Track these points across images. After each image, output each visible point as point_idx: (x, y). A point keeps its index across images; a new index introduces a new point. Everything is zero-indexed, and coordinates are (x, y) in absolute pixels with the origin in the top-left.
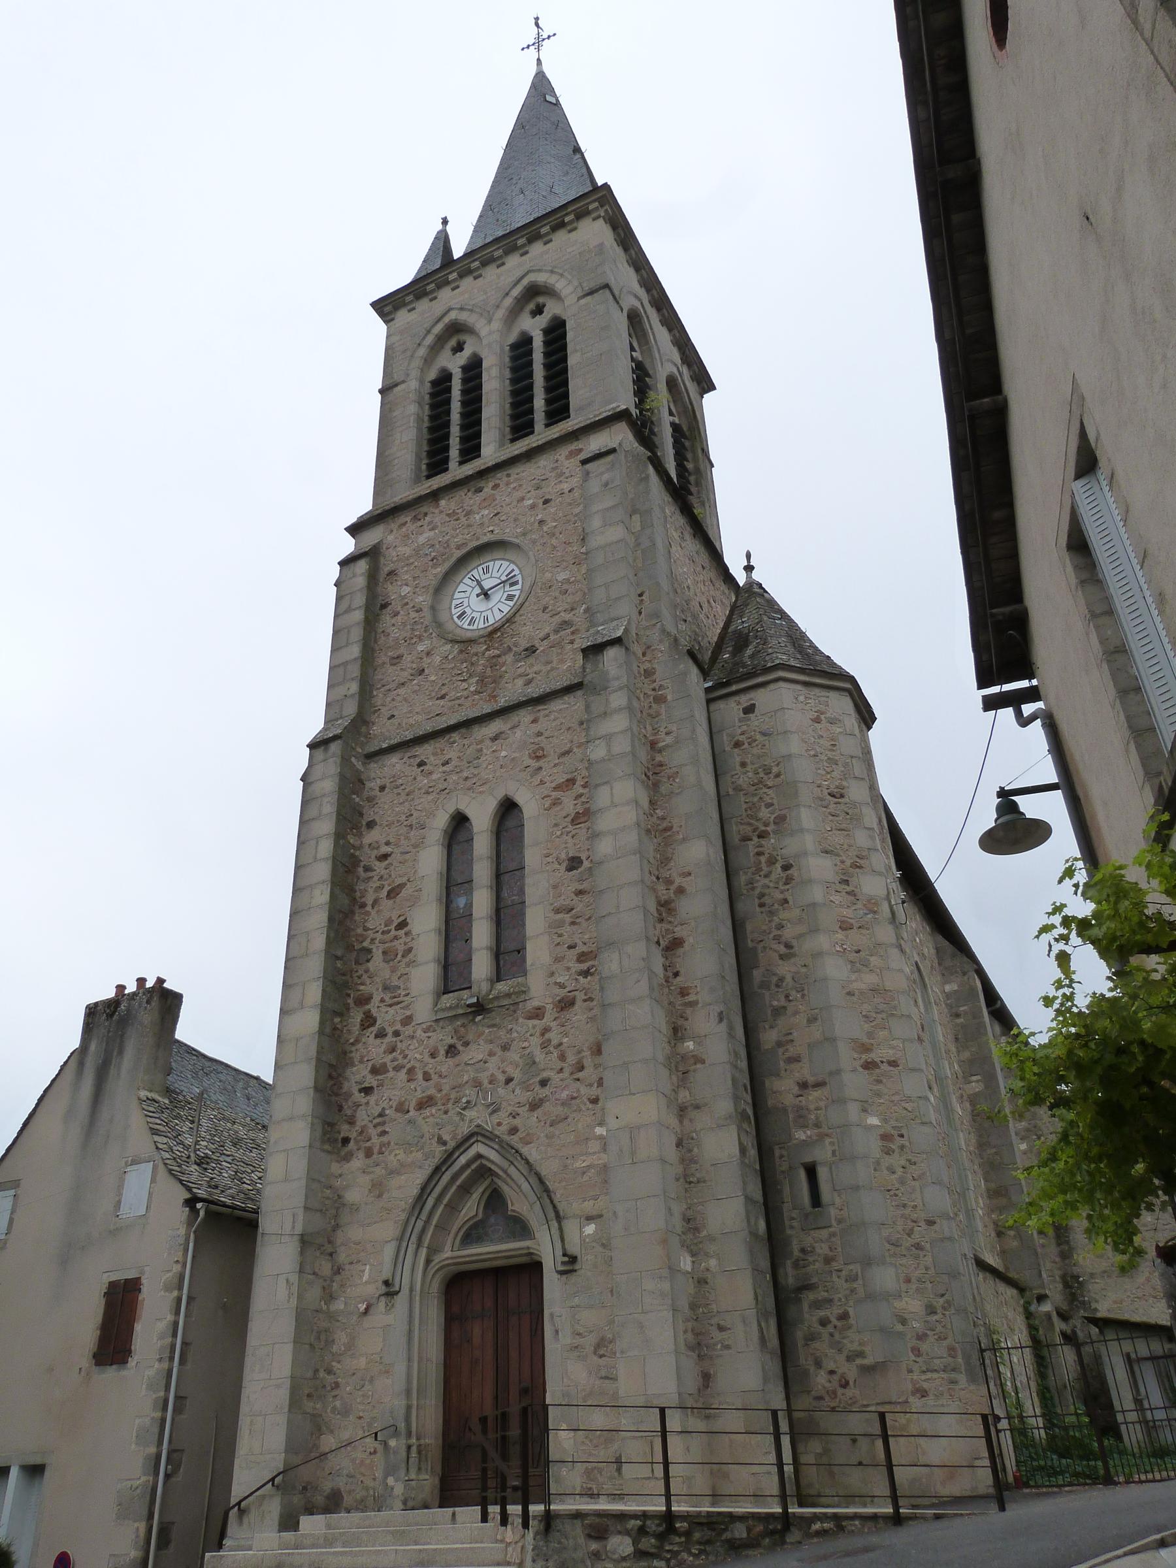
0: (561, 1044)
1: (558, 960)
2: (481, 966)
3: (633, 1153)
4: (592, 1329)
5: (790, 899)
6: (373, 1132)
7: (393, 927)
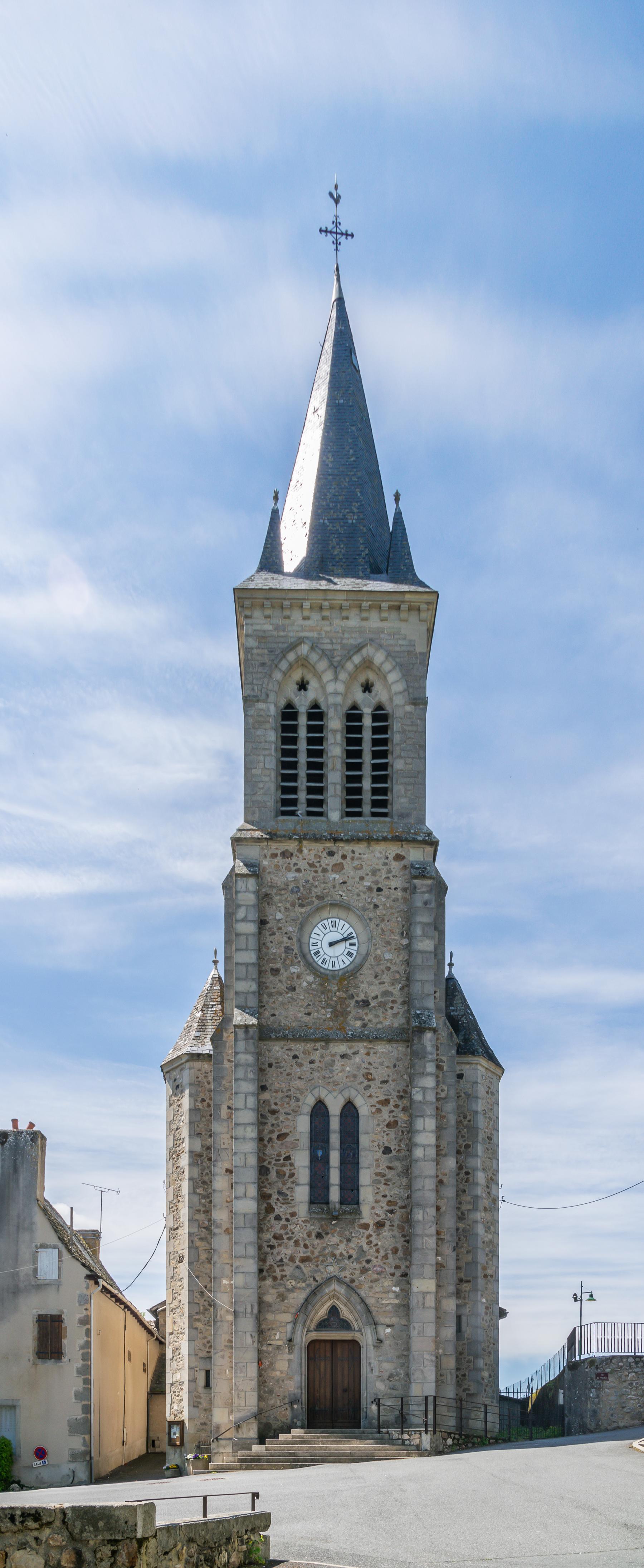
0: (377, 1245)
1: (377, 1202)
2: (335, 1195)
3: (424, 1304)
5: (467, 1190)
6: (277, 1269)
7: (282, 1158)
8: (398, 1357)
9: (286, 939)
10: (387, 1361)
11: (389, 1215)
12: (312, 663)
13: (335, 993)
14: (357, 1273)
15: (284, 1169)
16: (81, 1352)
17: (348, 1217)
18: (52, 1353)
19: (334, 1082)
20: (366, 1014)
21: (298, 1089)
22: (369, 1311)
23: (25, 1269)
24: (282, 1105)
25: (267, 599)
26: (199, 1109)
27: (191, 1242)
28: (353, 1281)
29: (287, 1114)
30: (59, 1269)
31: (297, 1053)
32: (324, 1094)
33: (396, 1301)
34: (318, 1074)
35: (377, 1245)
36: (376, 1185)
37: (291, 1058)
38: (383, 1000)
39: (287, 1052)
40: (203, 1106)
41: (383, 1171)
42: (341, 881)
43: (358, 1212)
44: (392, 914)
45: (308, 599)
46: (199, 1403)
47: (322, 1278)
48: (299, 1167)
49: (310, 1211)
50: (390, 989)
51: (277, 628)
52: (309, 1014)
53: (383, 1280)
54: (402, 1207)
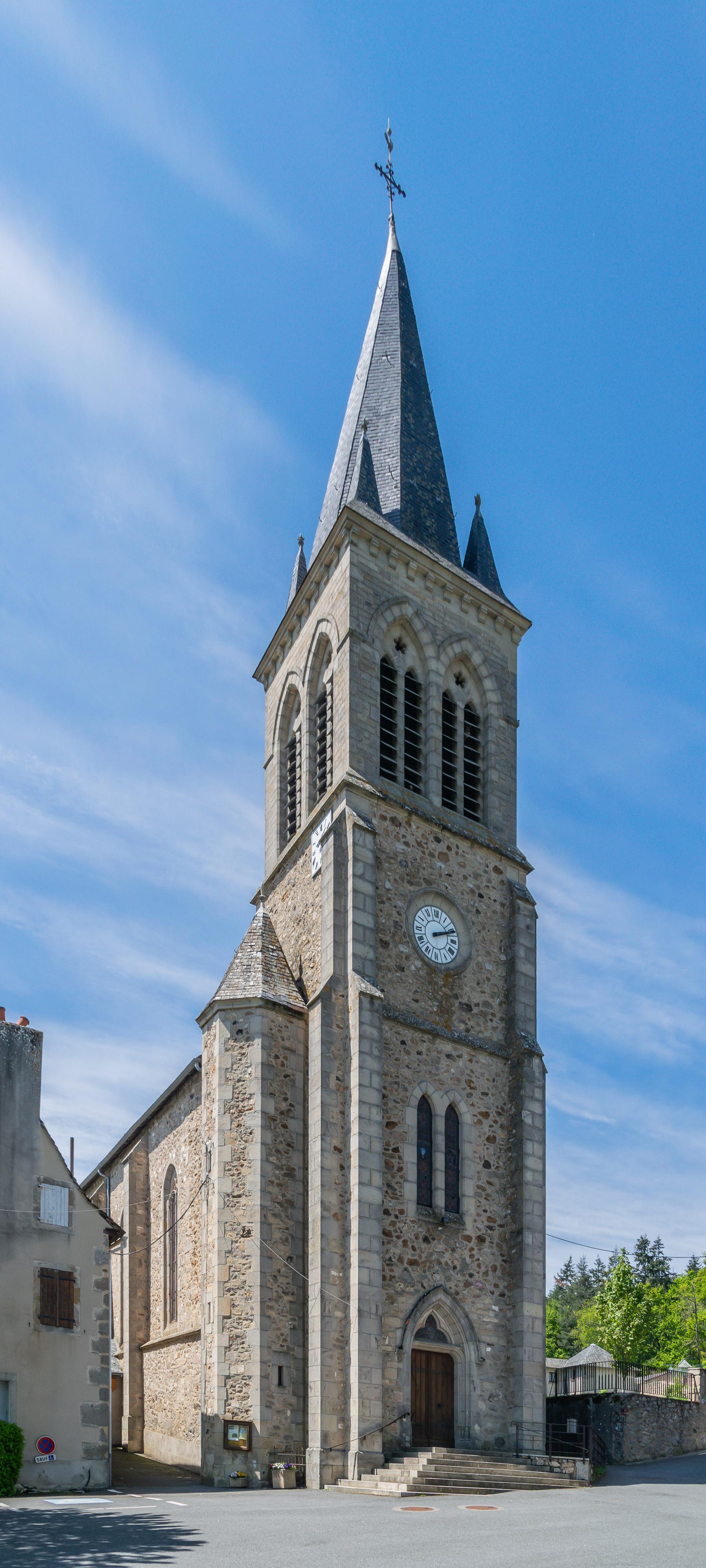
0: (478, 1260)
1: (478, 1215)
2: (440, 1199)
3: (533, 1328)
7: (391, 1148)
8: (498, 1378)
9: (395, 913)
10: (488, 1381)
11: (489, 1231)
12: (416, 630)
13: (441, 987)
14: (461, 1285)
15: (393, 1161)
16: (99, 1322)
17: (453, 1225)
18: (60, 1319)
19: (439, 1080)
20: (469, 1019)
21: (406, 1078)
22: (472, 1327)
23: (23, 1208)
24: (391, 1091)
25: (376, 536)
26: (273, 1066)
27: (264, 1216)
28: (457, 1293)
29: (395, 1101)
30: (70, 1215)
31: (405, 1039)
32: (431, 1090)
33: (496, 1321)
34: (425, 1068)
35: (478, 1260)
36: (478, 1198)
37: (399, 1043)
38: (483, 1009)
39: (395, 1034)
40: (277, 1064)
41: (484, 1185)
42: (447, 873)
43: (461, 1222)
44: (492, 925)
45: (416, 561)
46: (271, 1403)
47: (430, 1286)
48: (407, 1162)
49: (419, 1213)
50: (490, 1000)
51: (382, 572)
52: (417, 1001)
53: (484, 1297)
54: (501, 1226)
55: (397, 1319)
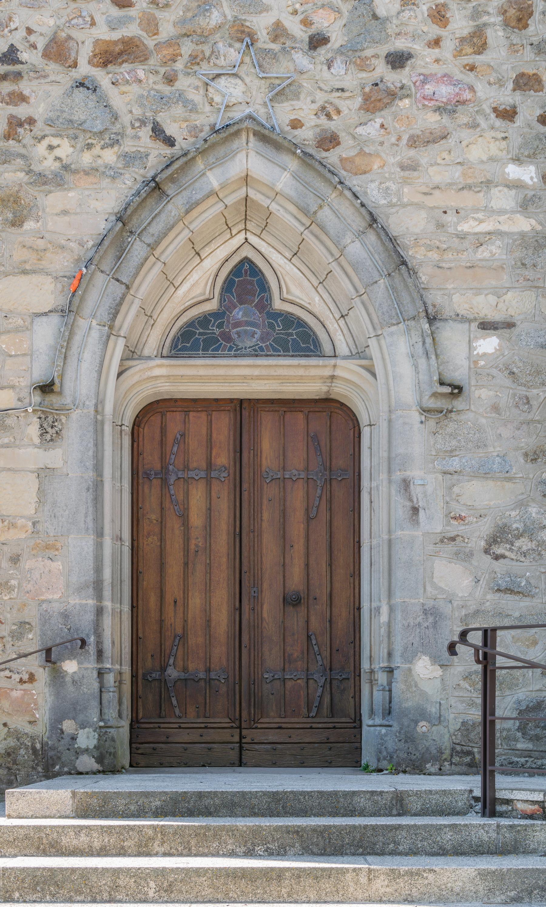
4: (483, 512)
47: (194, 130)
55: (35, 279)
